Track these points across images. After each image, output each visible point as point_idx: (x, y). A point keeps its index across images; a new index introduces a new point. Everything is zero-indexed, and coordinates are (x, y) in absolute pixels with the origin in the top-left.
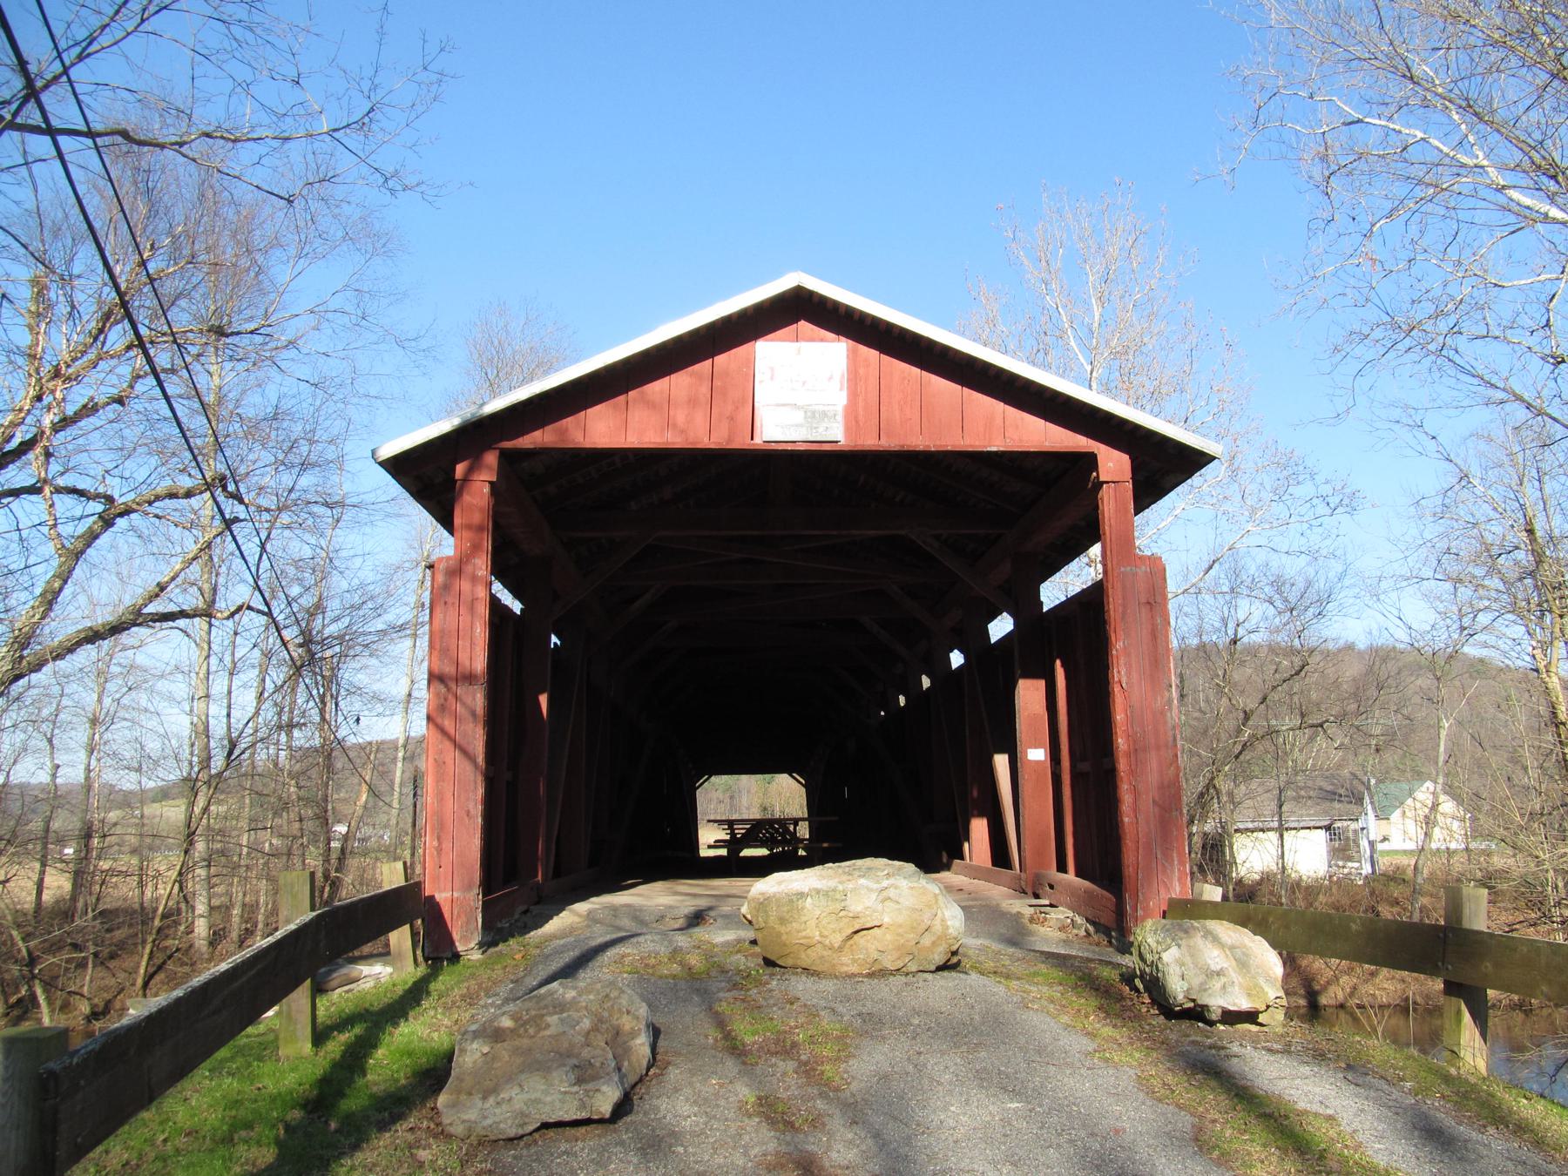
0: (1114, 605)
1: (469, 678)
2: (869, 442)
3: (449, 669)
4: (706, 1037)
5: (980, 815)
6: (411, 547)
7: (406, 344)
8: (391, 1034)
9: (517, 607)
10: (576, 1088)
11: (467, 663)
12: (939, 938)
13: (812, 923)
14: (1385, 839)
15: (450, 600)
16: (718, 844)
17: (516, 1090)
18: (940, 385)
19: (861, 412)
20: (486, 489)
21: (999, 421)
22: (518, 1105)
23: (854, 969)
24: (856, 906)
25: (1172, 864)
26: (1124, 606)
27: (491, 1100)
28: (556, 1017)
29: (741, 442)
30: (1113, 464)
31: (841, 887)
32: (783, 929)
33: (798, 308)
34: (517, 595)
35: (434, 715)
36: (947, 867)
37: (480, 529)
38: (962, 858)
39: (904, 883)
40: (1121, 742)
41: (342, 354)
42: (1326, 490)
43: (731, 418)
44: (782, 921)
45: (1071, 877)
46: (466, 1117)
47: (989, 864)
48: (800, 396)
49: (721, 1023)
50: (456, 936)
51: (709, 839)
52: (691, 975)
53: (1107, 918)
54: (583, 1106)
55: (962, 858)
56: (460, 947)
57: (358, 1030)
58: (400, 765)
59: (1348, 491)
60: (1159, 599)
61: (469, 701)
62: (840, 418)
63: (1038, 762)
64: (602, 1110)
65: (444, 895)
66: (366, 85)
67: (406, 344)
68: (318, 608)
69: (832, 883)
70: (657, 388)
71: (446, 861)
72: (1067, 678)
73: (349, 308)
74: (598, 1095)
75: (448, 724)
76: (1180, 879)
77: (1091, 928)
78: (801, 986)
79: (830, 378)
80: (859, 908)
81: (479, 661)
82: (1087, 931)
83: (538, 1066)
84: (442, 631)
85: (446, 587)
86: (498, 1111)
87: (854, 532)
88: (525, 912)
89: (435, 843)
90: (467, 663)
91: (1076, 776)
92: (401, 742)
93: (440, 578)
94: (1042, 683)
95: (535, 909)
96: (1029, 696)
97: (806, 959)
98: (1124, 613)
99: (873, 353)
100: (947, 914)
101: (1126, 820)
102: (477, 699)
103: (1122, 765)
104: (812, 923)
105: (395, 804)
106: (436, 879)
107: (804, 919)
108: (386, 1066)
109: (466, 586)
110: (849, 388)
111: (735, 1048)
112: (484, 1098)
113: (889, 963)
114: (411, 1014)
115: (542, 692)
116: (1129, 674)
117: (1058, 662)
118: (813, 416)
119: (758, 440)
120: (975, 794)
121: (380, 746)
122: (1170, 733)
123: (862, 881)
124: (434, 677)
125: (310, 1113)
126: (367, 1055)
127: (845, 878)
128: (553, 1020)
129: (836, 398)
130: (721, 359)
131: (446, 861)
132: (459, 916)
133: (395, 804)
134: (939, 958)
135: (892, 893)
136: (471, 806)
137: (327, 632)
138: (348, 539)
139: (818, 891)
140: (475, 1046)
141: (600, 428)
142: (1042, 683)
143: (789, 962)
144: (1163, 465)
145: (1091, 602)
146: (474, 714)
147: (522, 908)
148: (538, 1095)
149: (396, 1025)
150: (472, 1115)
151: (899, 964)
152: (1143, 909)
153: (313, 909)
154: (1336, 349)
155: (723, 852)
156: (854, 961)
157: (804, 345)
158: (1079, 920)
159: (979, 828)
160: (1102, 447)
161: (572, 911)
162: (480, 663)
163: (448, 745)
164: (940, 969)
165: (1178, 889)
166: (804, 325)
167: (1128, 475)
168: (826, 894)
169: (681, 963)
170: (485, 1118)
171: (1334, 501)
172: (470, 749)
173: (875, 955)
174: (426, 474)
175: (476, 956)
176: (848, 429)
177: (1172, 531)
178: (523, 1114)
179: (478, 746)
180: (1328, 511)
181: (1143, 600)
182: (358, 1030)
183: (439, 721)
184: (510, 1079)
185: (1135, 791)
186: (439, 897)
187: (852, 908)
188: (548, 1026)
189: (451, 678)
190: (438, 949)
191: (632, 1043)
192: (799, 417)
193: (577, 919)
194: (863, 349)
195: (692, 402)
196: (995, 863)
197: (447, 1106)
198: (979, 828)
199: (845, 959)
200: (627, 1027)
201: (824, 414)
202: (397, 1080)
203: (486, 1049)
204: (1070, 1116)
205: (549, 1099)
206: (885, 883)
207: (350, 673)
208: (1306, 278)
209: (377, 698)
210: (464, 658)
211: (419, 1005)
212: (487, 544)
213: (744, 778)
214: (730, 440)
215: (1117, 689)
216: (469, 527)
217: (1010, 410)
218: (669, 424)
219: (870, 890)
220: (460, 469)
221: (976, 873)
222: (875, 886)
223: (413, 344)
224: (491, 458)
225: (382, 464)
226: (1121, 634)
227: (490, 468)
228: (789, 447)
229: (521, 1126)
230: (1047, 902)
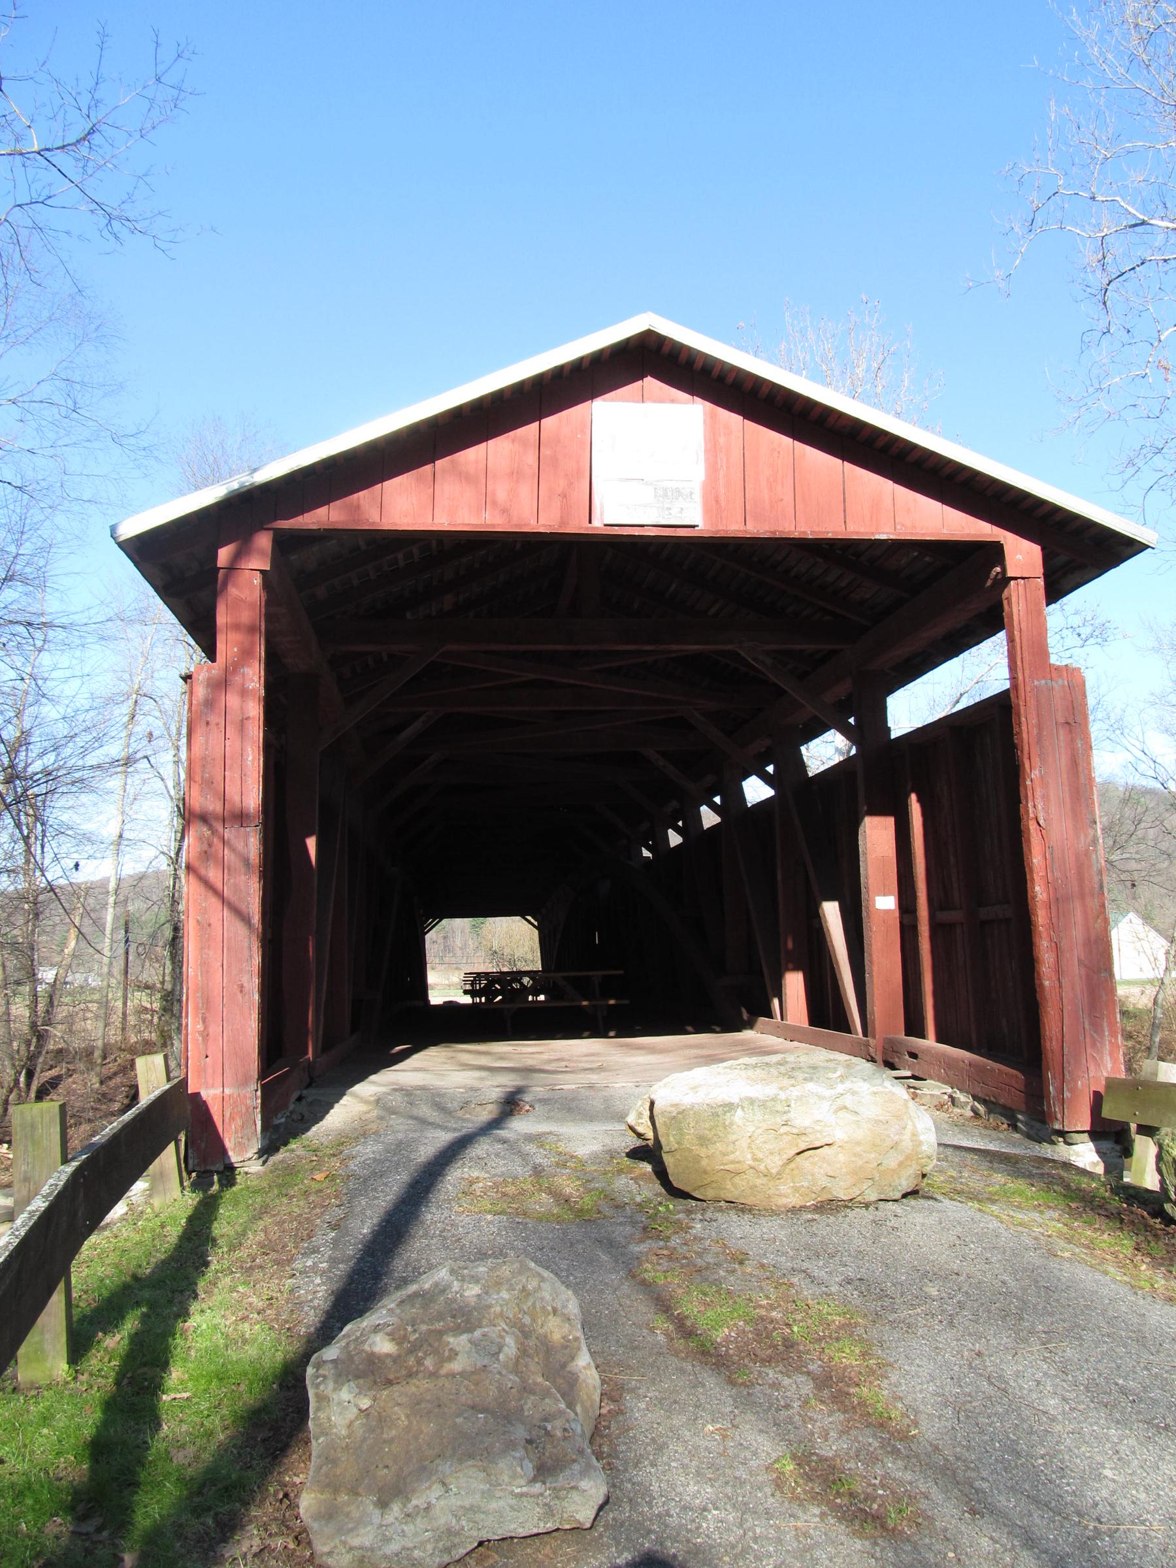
1: (241, 817)
2: (734, 526)
3: (213, 806)
4: (652, 1330)
5: (796, 969)
6: (120, 679)
7: (125, 441)
8: (184, 1332)
10: (537, 1488)
11: (237, 798)
12: (908, 1158)
13: (744, 1143)
15: (213, 719)
17: (437, 1490)
18: (817, 461)
19: (722, 491)
20: (257, 580)
21: (888, 502)
22: (443, 1519)
23: (794, 1201)
24: (801, 1118)
25: (1102, 1035)
26: (1040, 727)
27: (396, 1508)
28: (464, 1337)
29: (576, 525)
30: (1023, 556)
31: (782, 1096)
32: (703, 1152)
33: (648, 359)
35: (196, 863)
36: (750, 1025)
37: (251, 629)
38: (770, 1015)
39: (863, 1087)
40: (1039, 891)
41: (51, 451)
42: (1075, 621)
43: (564, 496)
44: (703, 1140)
45: (930, 1042)
46: (356, 1542)
47: (805, 1023)
48: (649, 471)
49: (663, 1304)
50: (228, 1144)
51: (445, 986)
52: (585, 1218)
53: (1014, 1097)
54: (549, 1512)
55: (770, 1015)
56: (234, 1158)
57: (131, 1324)
58: (111, 910)
59: (1097, 622)
60: (1078, 719)
61: (240, 846)
63: (887, 912)
64: (580, 1517)
65: (212, 1092)
66: (85, 100)
67: (125, 441)
68: (24, 740)
69: (770, 1090)
70: (472, 456)
71: (214, 1049)
72: (924, 814)
73: (58, 398)
74: (575, 1495)
75: (213, 874)
76: (1111, 1054)
77: (981, 1109)
78: (737, 1229)
80: (807, 1122)
81: (251, 794)
82: (973, 1110)
83: (470, 1448)
84: (204, 758)
85: (209, 703)
86: (409, 1529)
87: (674, 647)
88: (300, 1099)
89: (200, 1027)
90: (237, 798)
91: (936, 928)
92: (112, 886)
93: (201, 692)
94: (890, 821)
95: (312, 1094)
96: (876, 836)
97: (733, 1189)
98: (1040, 734)
99: (735, 419)
100: (920, 1126)
101: (1047, 983)
102: (251, 843)
103: (1041, 918)
104: (744, 1143)
105: (107, 952)
106: (201, 1071)
107: (733, 1137)
108: (193, 1404)
109: (233, 700)
110: (707, 460)
111: (705, 1353)
112: (383, 1504)
113: (841, 1192)
114: (201, 1284)
115: (310, 835)
116: (1047, 811)
117: (913, 797)
119: (597, 523)
120: (790, 945)
121: (89, 889)
122: (1096, 879)
123: (810, 1086)
124: (188, 816)
125: (81, 1519)
126: (154, 1387)
127: (786, 1082)
128: (459, 1342)
129: (694, 473)
130: (549, 422)
131: (214, 1049)
132: (232, 1118)
133: (107, 952)
134: (906, 1185)
135: (848, 1100)
136: (245, 979)
137: (30, 770)
138: (52, 662)
139: (752, 1101)
140: (345, 1394)
141: (404, 505)
142: (890, 821)
143: (710, 1194)
145: (989, 728)
146: (246, 861)
147: (295, 1095)
148: (476, 1499)
149: (184, 1314)
150: (364, 1538)
151: (854, 1192)
152: (1070, 1090)
153: (65, 1161)
154: (1131, 463)
156: (796, 1190)
157: (649, 407)
158: (961, 1097)
159: (794, 984)
160: (1009, 535)
161: (355, 1096)
162: (252, 797)
163: (214, 901)
164: (905, 1196)
165: (1109, 1065)
166: (650, 382)
167: (1039, 570)
168: (763, 1105)
169: (550, 1192)
170: (387, 1540)
171: (1086, 631)
172: (243, 907)
173: (823, 1182)
174: (179, 564)
175: (255, 1167)
176: (707, 511)
177: (1092, 634)
178: (450, 1532)
179: (254, 905)
180: (1079, 642)
181: (1061, 720)
182: (131, 1324)
183: (203, 872)
184: (424, 1471)
185: (1057, 948)
186: (204, 1094)
187: (797, 1123)
188: (454, 1354)
189: (216, 818)
190: (209, 1166)
191: (572, 1367)
193: (363, 1108)
194: (722, 413)
195: (516, 474)
196: (812, 1023)
197: (317, 1517)
198: (794, 984)
199: (784, 1189)
200: (557, 1337)
201: (678, 492)
202: (210, 1434)
203: (365, 1403)
205: (494, 1505)
206: (840, 1088)
207: (62, 810)
208: (1091, 390)
209: (88, 838)
210: (233, 792)
211: (207, 1264)
212: (261, 650)
213: (458, 920)
214: (563, 523)
215: (1033, 826)
216: (237, 627)
217: (902, 492)
218: (487, 500)
219: (821, 1098)
220: (224, 555)
221: (793, 1034)
222: (828, 1093)
223: (132, 441)
224: (264, 541)
225: (123, 545)
226: (1036, 760)
227: (262, 553)
228: (637, 532)
229: (448, 1550)
230: (908, 1074)
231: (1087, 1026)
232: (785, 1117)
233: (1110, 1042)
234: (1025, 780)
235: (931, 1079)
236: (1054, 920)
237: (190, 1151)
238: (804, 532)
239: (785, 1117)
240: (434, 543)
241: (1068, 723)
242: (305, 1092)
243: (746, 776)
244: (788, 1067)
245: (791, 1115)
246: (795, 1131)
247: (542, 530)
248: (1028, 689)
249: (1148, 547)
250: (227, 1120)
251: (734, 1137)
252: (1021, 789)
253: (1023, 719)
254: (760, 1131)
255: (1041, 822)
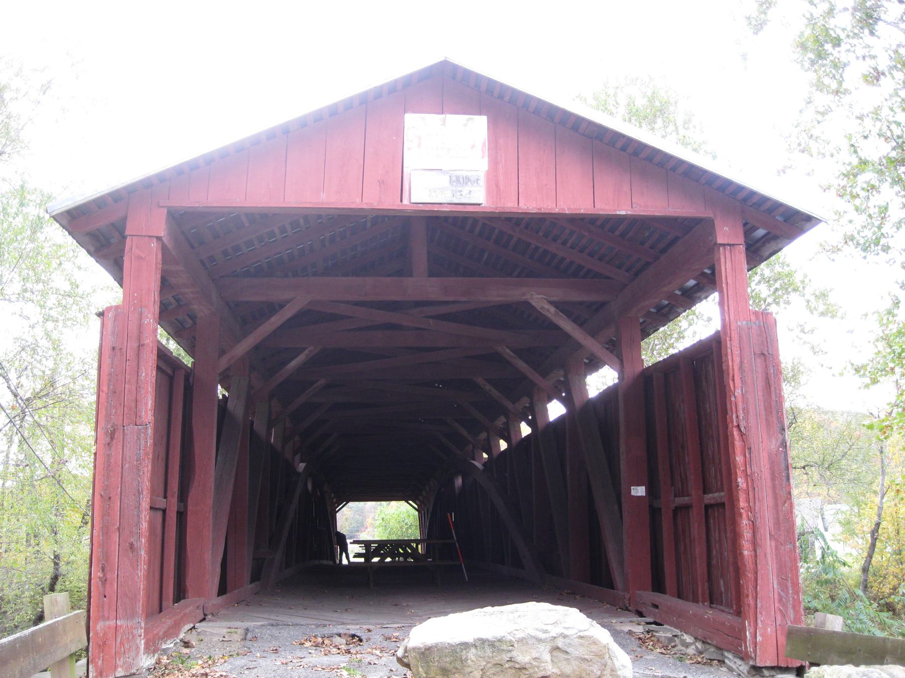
0: (734, 359)
2: (509, 205)
9: (188, 361)
14: (804, 16)
16: (358, 555)
29: (389, 203)
34: (191, 351)
62: (482, 182)
79: (473, 147)
89: (100, 574)
101: (746, 553)
118: (460, 181)
144: (770, 226)
155: (362, 560)
165: (792, 616)
181: (758, 352)
192: (444, 180)
204: (61, 425)
230: (651, 620)
231: (776, 586)
232: (509, 655)
233: (793, 598)
234: (730, 397)
235: (668, 624)
236: (751, 504)
237: (90, 667)
238: (563, 209)
239: (509, 655)
240: (302, 221)
241: (763, 354)
242: (197, 625)
243: (550, 400)
244: (516, 614)
245: (514, 654)
246: (517, 666)
247: (364, 207)
248: (732, 328)
249: (820, 221)
250: (118, 644)
251: (469, 670)
252: (728, 404)
253: (729, 351)
254: (489, 665)
255: (742, 429)
